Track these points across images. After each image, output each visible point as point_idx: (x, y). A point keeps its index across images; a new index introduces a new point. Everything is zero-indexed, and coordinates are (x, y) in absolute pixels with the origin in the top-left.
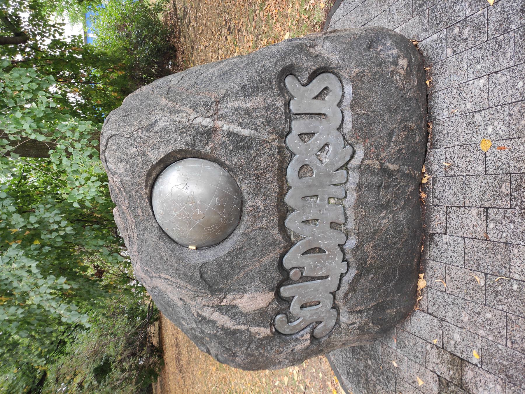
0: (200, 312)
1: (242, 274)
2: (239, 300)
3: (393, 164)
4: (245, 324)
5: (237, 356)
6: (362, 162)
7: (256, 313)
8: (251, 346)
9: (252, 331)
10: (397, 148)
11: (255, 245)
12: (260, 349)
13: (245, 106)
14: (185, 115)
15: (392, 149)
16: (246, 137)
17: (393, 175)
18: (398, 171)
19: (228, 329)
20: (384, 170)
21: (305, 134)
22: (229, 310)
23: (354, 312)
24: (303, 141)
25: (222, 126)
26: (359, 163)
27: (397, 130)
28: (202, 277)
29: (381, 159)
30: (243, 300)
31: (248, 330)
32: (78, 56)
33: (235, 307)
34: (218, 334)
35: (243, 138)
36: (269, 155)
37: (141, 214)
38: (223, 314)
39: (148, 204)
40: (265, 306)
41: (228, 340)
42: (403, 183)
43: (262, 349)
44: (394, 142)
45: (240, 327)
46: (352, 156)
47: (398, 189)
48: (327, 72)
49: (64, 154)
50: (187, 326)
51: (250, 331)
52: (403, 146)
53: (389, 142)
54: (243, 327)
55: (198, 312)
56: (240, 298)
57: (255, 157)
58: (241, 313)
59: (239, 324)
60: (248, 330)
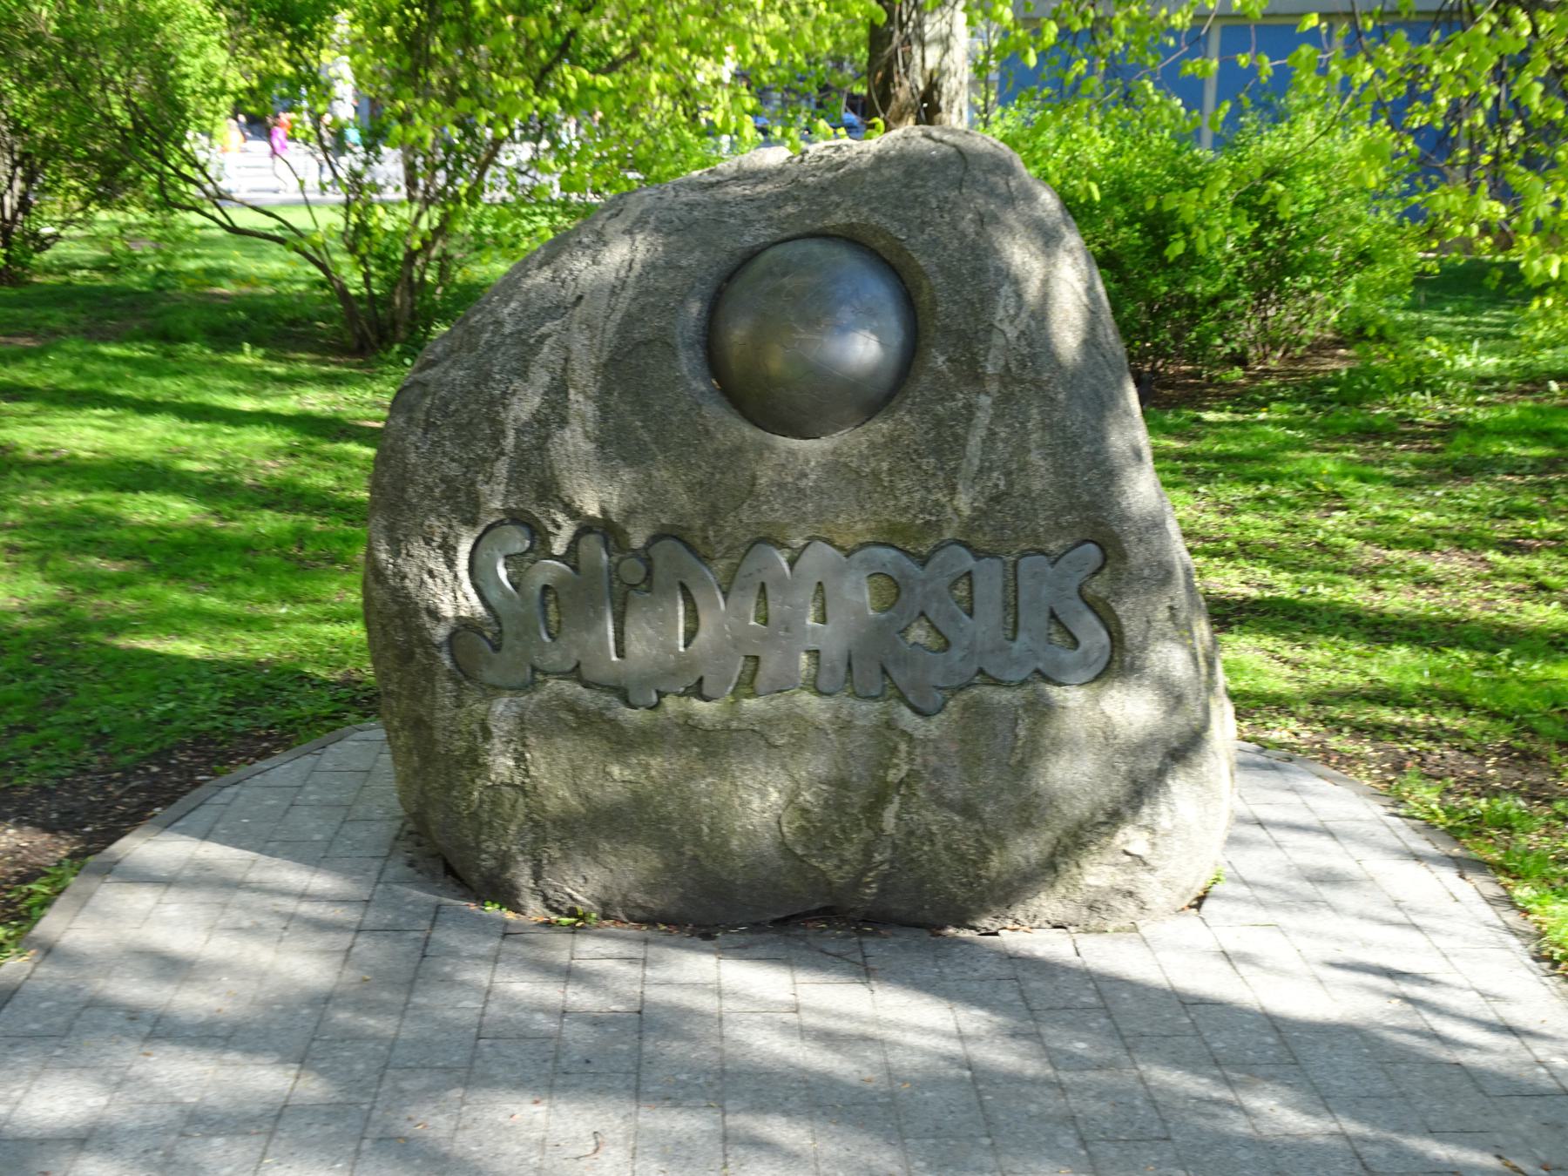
0: (549, 341)
1: (646, 437)
2: (580, 430)
3: (898, 817)
4: (517, 446)
5: (426, 432)
6: (904, 733)
7: (543, 471)
8: (454, 464)
9: (499, 464)
10: (934, 828)
11: (714, 468)
12: (443, 486)
13: (1033, 446)
14: (1012, 312)
15: (933, 818)
16: (964, 447)
17: (868, 819)
18: (879, 832)
19: (505, 407)
20: (879, 799)
21: (971, 592)
22: (553, 408)
23: (523, 730)
24: (953, 585)
25: (987, 394)
26: (902, 725)
27: (978, 826)
28: (638, 344)
29: (909, 786)
30: (580, 439)
31: (502, 453)
32: (1027, 167)
33: (563, 422)
34: (492, 384)
35: (960, 441)
36: (923, 500)
37: (782, 213)
38: (546, 393)
39: (808, 229)
40: (562, 494)
41: (473, 406)
42: (851, 852)
43: (443, 492)
44: (951, 820)
45: (511, 434)
46: (917, 711)
47: (833, 838)
48: (1113, 647)
49: (1514, 824)
50: (506, 311)
51: (497, 459)
52: (939, 845)
53: (950, 806)
54: (510, 441)
55: (549, 335)
56: (586, 433)
57: (919, 467)
58: (548, 436)
59: (518, 431)
60: (502, 453)
